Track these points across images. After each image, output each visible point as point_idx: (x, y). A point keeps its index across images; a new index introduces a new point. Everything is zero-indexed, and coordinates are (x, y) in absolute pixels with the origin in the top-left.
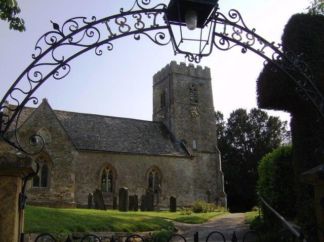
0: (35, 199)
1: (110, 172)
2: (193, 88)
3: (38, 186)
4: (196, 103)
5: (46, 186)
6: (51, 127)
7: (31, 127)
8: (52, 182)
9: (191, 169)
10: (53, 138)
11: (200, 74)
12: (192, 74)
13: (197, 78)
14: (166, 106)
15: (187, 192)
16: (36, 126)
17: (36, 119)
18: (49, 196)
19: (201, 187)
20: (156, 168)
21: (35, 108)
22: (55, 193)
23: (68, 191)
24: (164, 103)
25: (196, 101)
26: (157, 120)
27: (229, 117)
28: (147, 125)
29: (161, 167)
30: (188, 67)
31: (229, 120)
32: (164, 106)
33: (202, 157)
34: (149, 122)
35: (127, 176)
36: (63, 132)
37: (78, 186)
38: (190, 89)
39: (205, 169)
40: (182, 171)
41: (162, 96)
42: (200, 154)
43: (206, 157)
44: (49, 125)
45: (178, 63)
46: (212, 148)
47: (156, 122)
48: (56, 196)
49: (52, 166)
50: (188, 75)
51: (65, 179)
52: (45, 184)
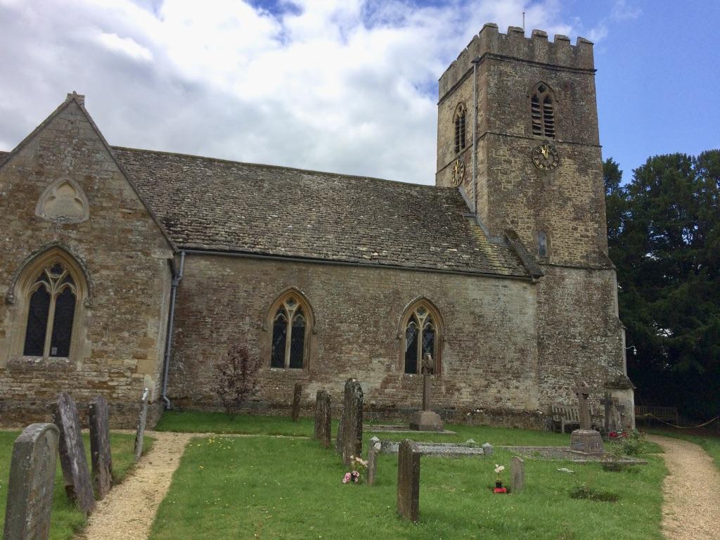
1: (299, 311)
2: (541, 96)
5: (66, 355)
6: (89, 178)
8: (82, 336)
9: (531, 311)
11: (562, 57)
12: (541, 55)
13: (553, 68)
16: (39, 173)
20: (426, 304)
26: (446, 184)
29: (441, 304)
30: (530, 41)
32: (463, 147)
33: (563, 278)
34: (430, 187)
41: (457, 123)
45: (503, 30)
48: (93, 386)
49: (85, 294)
50: (531, 63)
51: (126, 334)
52: (62, 347)
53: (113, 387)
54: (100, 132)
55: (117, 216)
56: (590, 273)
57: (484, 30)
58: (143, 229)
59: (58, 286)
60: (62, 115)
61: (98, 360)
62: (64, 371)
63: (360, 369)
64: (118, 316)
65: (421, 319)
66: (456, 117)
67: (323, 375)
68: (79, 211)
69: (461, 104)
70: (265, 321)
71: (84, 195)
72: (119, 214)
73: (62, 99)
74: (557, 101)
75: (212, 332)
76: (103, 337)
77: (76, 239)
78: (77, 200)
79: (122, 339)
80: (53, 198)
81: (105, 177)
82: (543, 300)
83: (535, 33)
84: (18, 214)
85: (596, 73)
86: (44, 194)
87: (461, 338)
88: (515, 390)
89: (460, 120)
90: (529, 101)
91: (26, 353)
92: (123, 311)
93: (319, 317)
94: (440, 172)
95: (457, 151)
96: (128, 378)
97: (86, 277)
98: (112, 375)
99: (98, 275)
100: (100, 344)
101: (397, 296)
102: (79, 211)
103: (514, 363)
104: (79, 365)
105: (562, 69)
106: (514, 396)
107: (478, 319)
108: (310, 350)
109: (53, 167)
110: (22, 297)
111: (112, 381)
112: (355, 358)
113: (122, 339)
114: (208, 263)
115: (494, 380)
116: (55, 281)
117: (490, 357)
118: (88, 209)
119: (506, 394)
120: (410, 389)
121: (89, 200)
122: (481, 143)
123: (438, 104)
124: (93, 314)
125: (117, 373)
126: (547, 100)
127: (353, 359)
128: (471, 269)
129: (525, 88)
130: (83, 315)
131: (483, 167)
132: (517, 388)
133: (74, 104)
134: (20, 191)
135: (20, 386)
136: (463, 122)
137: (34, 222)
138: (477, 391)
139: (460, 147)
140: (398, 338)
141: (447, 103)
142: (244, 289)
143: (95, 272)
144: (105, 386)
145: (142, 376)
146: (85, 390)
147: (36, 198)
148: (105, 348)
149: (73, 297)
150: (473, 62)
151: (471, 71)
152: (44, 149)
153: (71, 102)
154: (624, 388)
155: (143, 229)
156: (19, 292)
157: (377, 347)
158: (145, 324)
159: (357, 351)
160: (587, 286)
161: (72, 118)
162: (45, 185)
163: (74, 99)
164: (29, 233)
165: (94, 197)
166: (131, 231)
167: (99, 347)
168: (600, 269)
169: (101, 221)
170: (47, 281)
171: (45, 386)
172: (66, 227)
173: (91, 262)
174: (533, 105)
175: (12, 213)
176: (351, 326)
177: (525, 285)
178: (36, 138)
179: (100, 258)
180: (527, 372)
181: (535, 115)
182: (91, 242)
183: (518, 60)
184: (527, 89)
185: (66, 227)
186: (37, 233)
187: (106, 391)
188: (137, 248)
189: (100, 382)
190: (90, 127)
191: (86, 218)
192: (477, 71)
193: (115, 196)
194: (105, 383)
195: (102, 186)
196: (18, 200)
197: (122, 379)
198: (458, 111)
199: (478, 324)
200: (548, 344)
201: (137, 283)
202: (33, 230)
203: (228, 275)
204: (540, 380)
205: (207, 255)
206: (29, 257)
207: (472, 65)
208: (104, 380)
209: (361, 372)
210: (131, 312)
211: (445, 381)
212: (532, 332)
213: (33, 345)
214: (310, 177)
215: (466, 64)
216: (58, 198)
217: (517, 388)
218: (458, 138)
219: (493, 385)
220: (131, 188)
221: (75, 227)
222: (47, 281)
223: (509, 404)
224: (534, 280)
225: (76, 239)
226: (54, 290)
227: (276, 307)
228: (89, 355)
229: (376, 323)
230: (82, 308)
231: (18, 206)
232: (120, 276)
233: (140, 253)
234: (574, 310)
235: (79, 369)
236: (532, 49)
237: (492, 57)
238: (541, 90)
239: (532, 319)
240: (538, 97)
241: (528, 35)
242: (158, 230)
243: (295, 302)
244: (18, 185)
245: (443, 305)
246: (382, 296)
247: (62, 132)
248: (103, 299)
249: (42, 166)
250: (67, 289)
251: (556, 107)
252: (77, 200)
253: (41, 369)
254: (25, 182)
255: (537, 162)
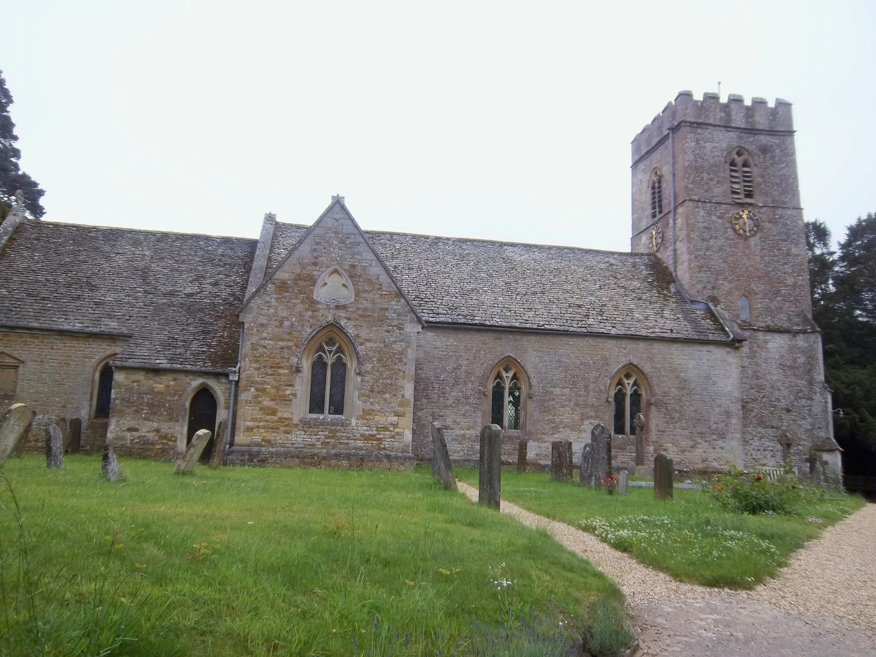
0: (314, 445)
1: (515, 377)
2: (739, 160)
3: (323, 413)
4: (749, 200)
5: (341, 413)
7: (303, 267)
9: (735, 373)
10: (357, 294)
11: (761, 122)
12: (739, 120)
13: (752, 131)
14: (665, 211)
15: (722, 436)
17: (314, 247)
18: (348, 438)
19: (761, 423)
21: (356, 226)
22: (363, 430)
23: (395, 426)
24: (660, 206)
25: (749, 195)
26: (642, 250)
27: (843, 239)
28: (613, 261)
30: (726, 106)
31: (843, 247)
32: (660, 212)
33: (766, 342)
35: (557, 391)
36: (384, 278)
37: (434, 413)
38: (733, 164)
39: (775, 375)
40: (708, 377)
41: (653, 188)
42: (760, 335)
43: (777, 343)
44: (349, 261)
45: (698, 97)
46: (796, 320)
47: (637, 254)
48: (367, 438)
49: (355, 363)
50: (727, 127)
51: (388, 396)
52: (338, 407)
53: (380, 439)
54: (320, 217)
55: (376, 297)
56: (794, 336)
57: (679, 99)
58: (397, 307)
59: (333, 357)
60: (330, 215)
61: (367, 417)
62: (342, 426)
63: (573, 430)
64: (381, 381)
65: (628, 384)
66: (651, 182)
67: (539, 436)
68: (347, 295)
69: (656, 169)
70: (485, 387)
71: (350, 281)
72: (377, 296)
73: (328, 202)
74: (756, 165)
75: (440, 397)
76: (370, 398)
77: (345, 318)
78: (344, 285)
79: (385, 400)
80: (326, 284)
81: (365, 265)
82: (746, 364)
83: (732, 98)
84: (301, 298)
85: (795, 134)
86: (319, 281)
87: (667, 401)
88: (720, 450)
89: (657, 185)
90: (727, 166)
91: (311, 411)
92: (385, 376)
93: (534, 382)
94: (635, 238)
95: (654, 216)
96: (391, 431)
97: (355, 349)
98: (379, 430)
99: (363, 347)
100: (368, 404)
101: (605, 362)
102: (347, 295)
103: (719, 425)
104: (354, 422)
105: (759, 132)
106: (719, 455)
107: (683, 385)
108: (526, 412)
109: (325, 259)
110: (306, 365)
111: (380, 434)
112: (569, 420)
113: (385, 400)
114: (434, 334)
115: (699, 440)
116: (330, 352)
117: (696, 419)
118: (353, 293)
119: (712, 455)
120: (619, 449)
121: (354, 285)
122: (680, 210)
123: (632, 167)
124: (362, 379)
125: (383, 427)
126: (745, 164)
127: (566, 421)
128: (674, 336)
129: (722, 154)
130: (353, 382)
131: (682, 235)
132: (722, 448)
133: (338, 204)
134: (301, 280)
135: (310, 438)
136: (660, 187)
137: (313, 305)
138: (683, 451)
139: (657, 213)
140: (607, 401)
141: (641, 166)
142: (466, 357)
143: (362, 344)
144: (374, 438)
145: (402, 431)
146: (359, 442)
147: (314, 283)
148: (372, 407)
149: (344, 365)
150: (669, 129)
151: (666, 137)
152: (317, 243)
153: (336, 203)
154: (831, 451)
155: (397, 307)
156: (305, 361)
157: (588, 410)
158: (402, 387)
159: (569, 413)
160: (792, 349)
161: (337, 217)
162: (320, 274)
163: (338, 201)
164: (310, 313)
165: (358, 281)
166: (387, 309)
167: (368, 406)
168: (804, 332)
169: (365, 302)
170: (324, 352)
171: (329, 437)
172: (337, 307)
173: (358, 336)
174: (732, 171)
175: (296, 298)
176: (563, 390)
177: (728, 349)
178: (310, 235)
179: (364, 333)
180: (732, 433)
181: (734, 180)
182: (357, 320)
183: (715, 126)
184: (725, 153)
185: (337, 307)
186: (316, 313)
187: (374, 442)
188: (393, 324)
189: (370, 435)
190: (351, 224)
191: (353, 300)
192: (673, 138)
193: (374, 281)
194: (374, 436)
195: (363, 273)
196: (300, 287)
197: (387, 433)
198: (653, 175)
199: (684, 388)
200: (753, 407)
201: (394, 353)
202: (313, 311)
203: (451, 345)
204: (745, 442)
205: (433, 327)
206: (312, 332)
207: (668, 131)
208: (373, 434)
209: (573, 432)
210: (390, 378)
211: (653, 442)
212: (737, 395)
213: (316, 405)
214: (512, 249)
215: (661, 132)
216: (329, 284)
217: (722, 448)
218: (654, 203)
219: (699, 446)
220: (386, 274)
221: (344, 307)
222: (324, 352)
223: (715, 464)
224: (737, 344)
225: (345, 318)
226: (330, 360)
227: (494, 374)
228: (361, 413)
229: (586, 386)
230: (353, 373)
231: (300, 292)
232: (381, 347)
233: (395, 328)
234: (647, 318)
235: (353, 424)
236: (728, 114)
237: (688, 124)
238: (739, 154)
239: (736, 382)
240: (736, 161)
241: (724, 100)
242: (409, 307)
243: (510, 369)
244: (299, 275)
245: (649, 370)
246: (591, 362)
247: (330, 229)
248: (368, 367)
249: (316, 258)
250: (339, 358)
251: (755, 171)
252: (344, 285)
253: (323, 423)
254: (304, 272)
255: (737, 227)
